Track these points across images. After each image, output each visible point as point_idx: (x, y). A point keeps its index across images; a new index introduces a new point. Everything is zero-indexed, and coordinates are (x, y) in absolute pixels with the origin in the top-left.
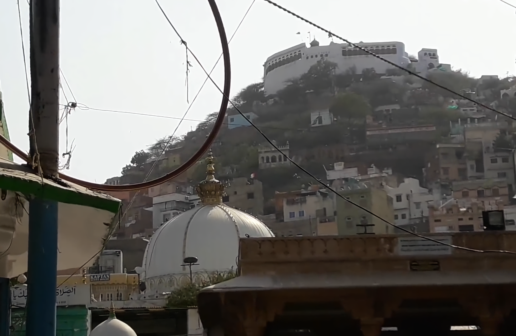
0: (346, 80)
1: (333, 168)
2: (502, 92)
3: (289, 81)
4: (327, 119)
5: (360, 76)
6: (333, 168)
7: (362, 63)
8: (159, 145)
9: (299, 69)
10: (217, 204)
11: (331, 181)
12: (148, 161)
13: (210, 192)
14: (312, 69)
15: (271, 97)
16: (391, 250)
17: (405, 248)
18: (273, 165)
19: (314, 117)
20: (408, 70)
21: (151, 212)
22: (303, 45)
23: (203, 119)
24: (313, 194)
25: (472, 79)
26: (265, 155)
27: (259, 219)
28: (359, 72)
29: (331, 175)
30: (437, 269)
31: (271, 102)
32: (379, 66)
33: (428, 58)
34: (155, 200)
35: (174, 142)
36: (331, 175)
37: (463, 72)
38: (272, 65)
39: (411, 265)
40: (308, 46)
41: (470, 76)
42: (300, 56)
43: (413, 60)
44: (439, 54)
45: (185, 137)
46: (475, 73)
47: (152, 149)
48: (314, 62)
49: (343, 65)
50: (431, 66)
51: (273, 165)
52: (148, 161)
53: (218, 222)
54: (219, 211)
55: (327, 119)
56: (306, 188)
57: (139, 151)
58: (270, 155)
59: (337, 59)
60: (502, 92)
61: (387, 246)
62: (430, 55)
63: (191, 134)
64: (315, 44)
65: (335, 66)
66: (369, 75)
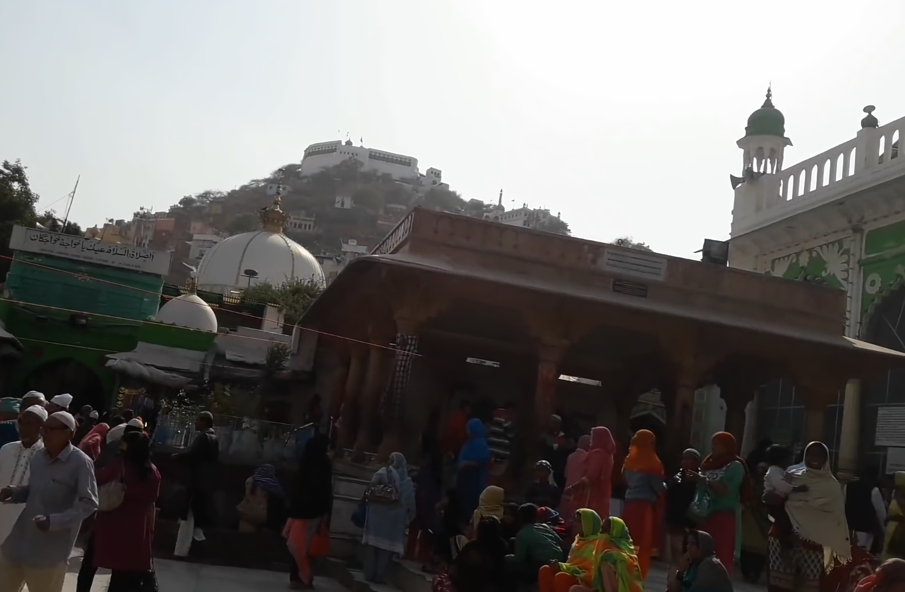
0: (369, 177)
1: (347, 243)
2: (485, 214)
3: (324, 168)
4: (348, 204)
5: (378, 178)
6: (347, 243)
7: (383, 168)
8: (206, 194)
9: (332, 161)
10: (277, 232)
11: (345, 253)
12: (194, 205)
13: (273, 220)
14: (344, 162)
15: (305, 177)
16: (594, 261)
17: (611, 262)
18: (299, 231)
19: (338, 199)
20: (418, 180)
21: (189, 246)
22: (340, 142)
23: (246, 183)
24: (330, 258)
25: (462, 200)
26: (294, 221)
27: (312, 253)
28: (379, 174)
29: (345, 248)
30: (645, 296)
31: (305, 181)
32: (397, 172)
33: (433, 175)
34: (195, 237)
35: (218, 195)
36: (345, 248)
37: (458, 194)
38: (311, 152)
39: (614, 284)
40: (344, 143)
41: (462, 197)
42: (335, 150)
43: (421, 175)
44: (442, 175)
45: (229, 194)
46: (466, 198)
47: (198, 197)
48: (347, 157)
49: (368, 166)
50: (434, 182)
51: (299, 231)
52: (194, 205)
53: (275, 247)
54: (278, 238)
55: (348, 204)
56: (324, 253)
57: (187, 195)
58: (298, 222)
59: (365, 160)
60: (485, 214)
61: (590, 256)
62: (435, 174)
63: (234, 192)
64: (349, 143)
65: (362, 164)
66: (386, 178)
